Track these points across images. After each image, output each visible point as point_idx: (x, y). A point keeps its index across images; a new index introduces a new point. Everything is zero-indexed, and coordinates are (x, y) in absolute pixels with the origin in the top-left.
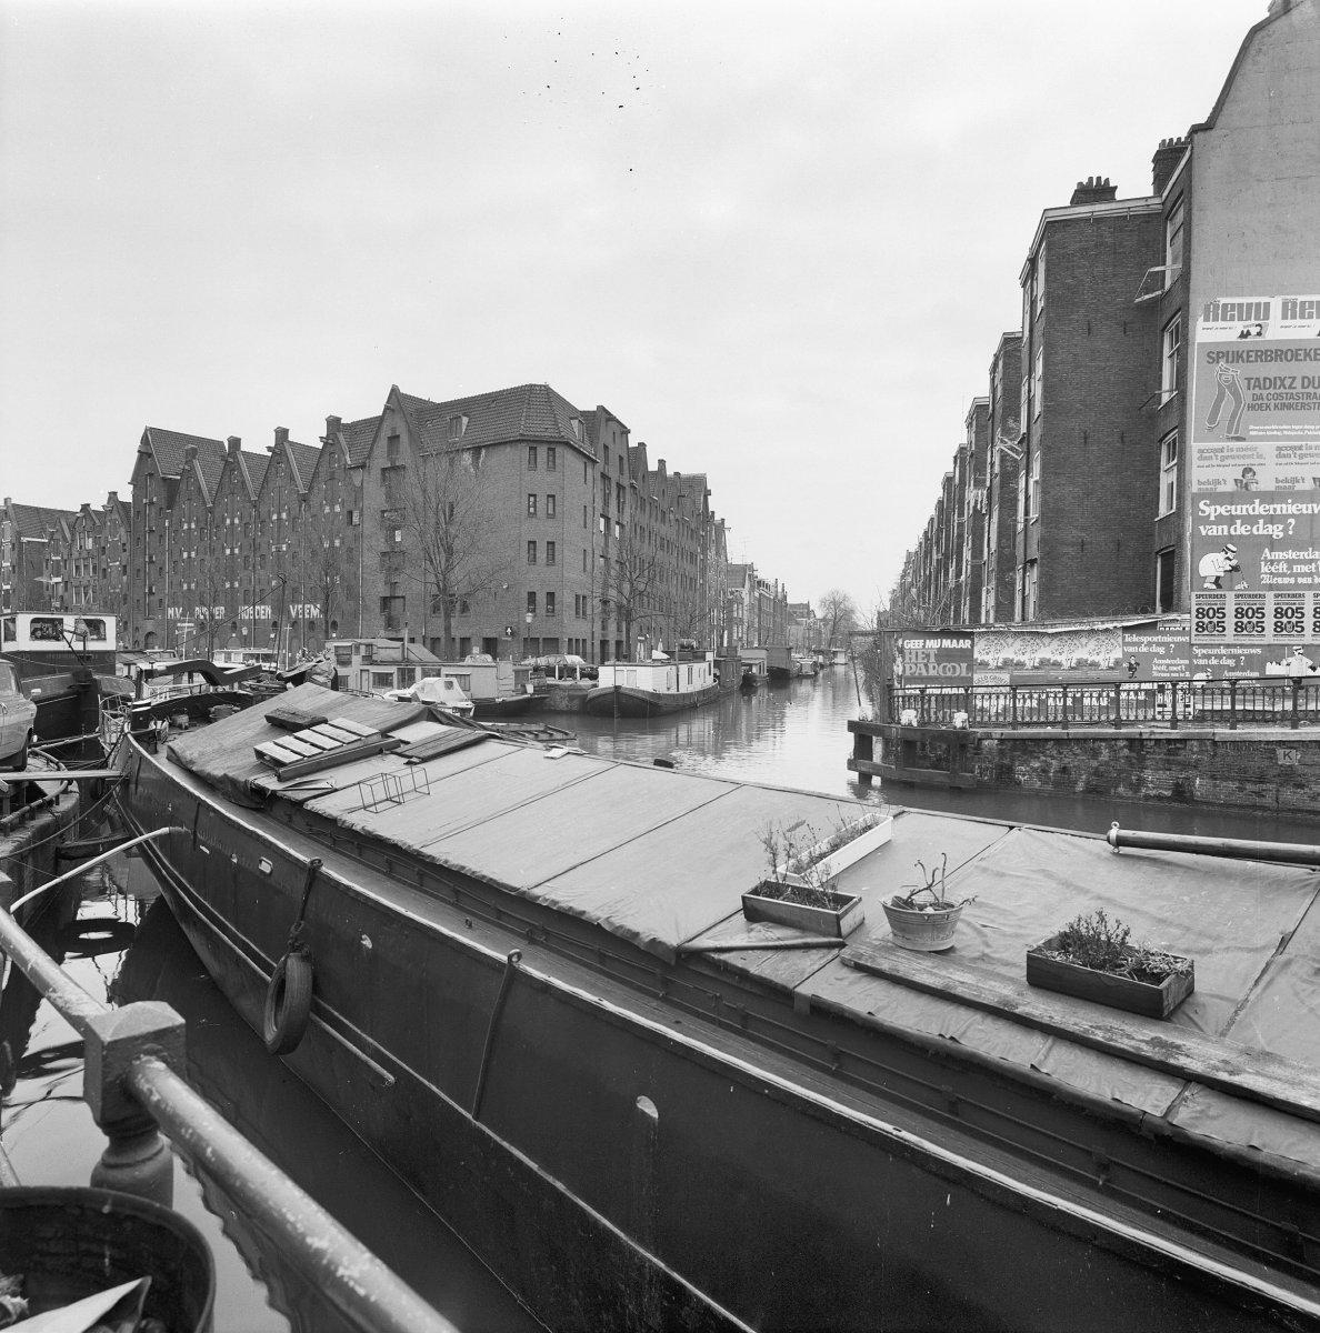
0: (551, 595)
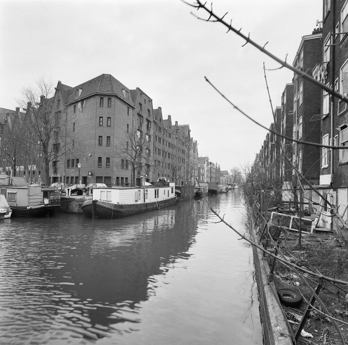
0: (108, 159)
